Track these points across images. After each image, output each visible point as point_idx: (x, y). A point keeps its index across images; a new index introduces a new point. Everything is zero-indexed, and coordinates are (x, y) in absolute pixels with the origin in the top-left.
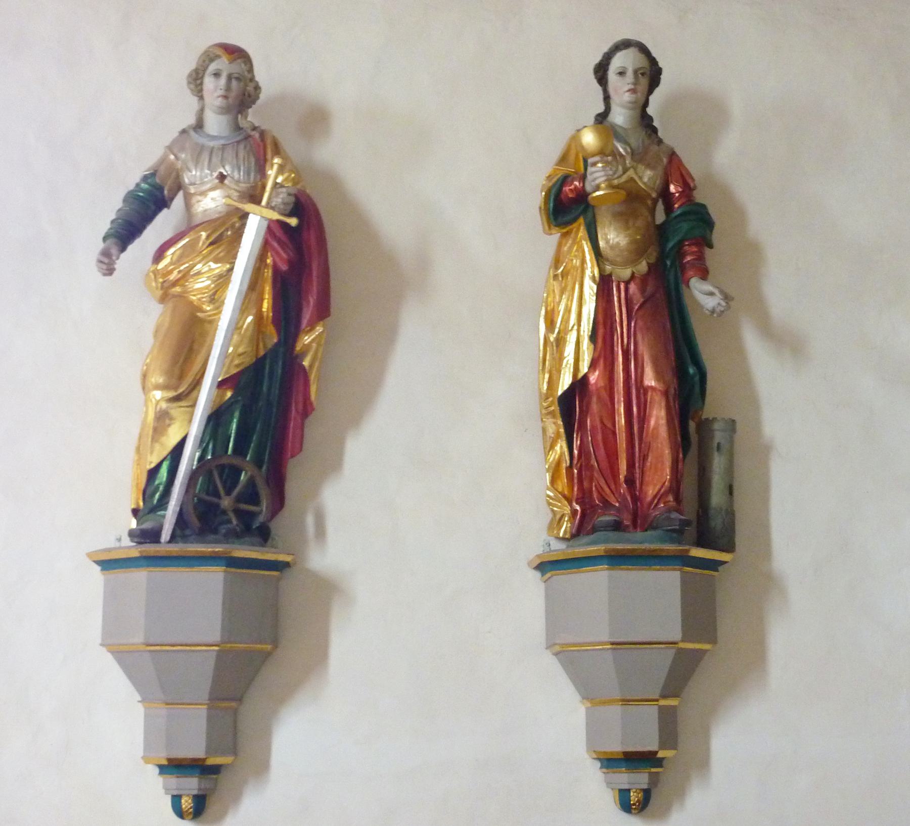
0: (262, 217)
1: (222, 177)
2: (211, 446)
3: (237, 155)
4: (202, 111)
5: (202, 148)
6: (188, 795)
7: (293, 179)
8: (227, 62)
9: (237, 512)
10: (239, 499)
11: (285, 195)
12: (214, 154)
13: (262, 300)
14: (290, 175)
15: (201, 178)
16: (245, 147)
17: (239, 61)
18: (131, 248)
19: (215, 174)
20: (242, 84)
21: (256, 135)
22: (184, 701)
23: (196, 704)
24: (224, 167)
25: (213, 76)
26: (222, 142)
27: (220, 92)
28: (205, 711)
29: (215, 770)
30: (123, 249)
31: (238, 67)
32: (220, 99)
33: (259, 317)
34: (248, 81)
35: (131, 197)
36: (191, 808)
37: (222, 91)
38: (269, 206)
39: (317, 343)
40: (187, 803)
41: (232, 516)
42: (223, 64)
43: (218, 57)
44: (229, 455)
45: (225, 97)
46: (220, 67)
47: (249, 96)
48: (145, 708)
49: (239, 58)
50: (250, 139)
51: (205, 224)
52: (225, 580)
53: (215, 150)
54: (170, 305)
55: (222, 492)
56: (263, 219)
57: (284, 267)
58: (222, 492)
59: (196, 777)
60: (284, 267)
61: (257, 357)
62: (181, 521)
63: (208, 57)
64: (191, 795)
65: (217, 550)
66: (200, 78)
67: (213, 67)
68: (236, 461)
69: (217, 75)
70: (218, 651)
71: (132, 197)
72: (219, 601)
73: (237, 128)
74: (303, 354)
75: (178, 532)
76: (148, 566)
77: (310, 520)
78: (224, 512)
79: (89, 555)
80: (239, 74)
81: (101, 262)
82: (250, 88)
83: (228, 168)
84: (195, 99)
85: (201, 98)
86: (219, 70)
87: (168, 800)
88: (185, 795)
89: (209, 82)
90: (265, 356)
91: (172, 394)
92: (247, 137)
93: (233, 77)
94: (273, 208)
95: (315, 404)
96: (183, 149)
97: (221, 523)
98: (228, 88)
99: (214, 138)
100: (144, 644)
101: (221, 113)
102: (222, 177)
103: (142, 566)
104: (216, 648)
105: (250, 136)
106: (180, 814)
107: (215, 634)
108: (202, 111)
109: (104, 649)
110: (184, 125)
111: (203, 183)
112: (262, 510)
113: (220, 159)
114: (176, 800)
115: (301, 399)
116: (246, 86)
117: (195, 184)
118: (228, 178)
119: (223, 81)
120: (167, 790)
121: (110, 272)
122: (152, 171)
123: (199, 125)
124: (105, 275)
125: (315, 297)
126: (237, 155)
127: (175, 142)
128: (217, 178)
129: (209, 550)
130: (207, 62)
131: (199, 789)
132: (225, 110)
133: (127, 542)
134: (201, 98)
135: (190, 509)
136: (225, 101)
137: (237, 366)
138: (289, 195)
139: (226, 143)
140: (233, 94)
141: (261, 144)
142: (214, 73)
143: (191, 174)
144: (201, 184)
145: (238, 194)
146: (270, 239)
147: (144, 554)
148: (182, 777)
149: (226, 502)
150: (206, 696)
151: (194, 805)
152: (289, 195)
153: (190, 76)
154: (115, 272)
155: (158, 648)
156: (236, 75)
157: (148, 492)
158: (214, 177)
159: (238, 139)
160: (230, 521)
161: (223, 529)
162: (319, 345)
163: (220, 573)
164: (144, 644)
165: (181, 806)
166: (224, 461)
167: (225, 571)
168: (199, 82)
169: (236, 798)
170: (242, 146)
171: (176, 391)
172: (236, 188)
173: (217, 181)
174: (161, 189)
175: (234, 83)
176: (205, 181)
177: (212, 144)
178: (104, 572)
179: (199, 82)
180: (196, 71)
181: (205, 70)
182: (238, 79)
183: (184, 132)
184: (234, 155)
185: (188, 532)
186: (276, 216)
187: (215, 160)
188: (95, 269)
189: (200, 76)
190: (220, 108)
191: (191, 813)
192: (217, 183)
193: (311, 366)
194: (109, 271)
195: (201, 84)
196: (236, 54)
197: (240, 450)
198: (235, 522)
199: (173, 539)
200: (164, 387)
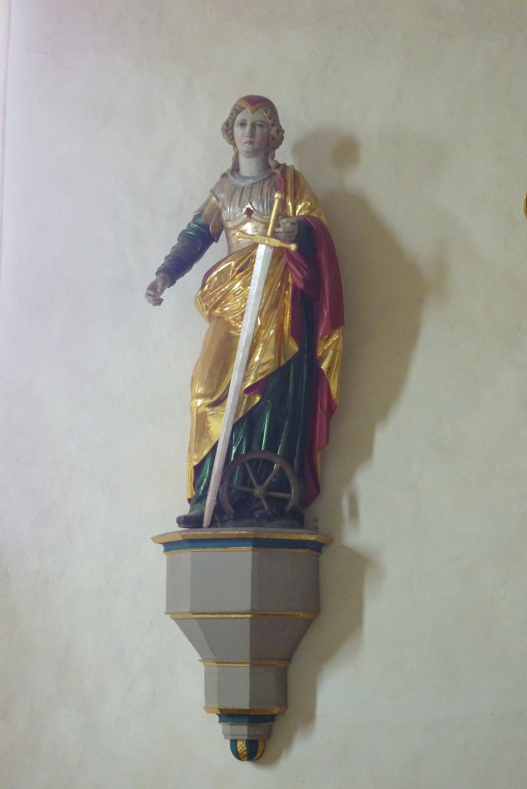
0: (268, 245)
1: (249, 212)
2: (244, 444)
3: (262, 191)
4: (237, 156)
5: (236, 187)
6: (242, 740)
7: (310, 206)
8: (250, 112)
9: (268, 498)
10: (270, 488)
11: (288, 225)
12: (244, 192)
13: (285, 315)
14: (307, 204)
15: (234, 214)
16: (270, 184)
17: (260, 110)
18: (180, 282)
19: (244, 210)
20: (265, 130)
21: (278, 172)
22: (232, 660)
23: (237, 663)
24: (251, 204)
25: (239, 126)
26: (251, 181)
27: (247, 139)
28: (249, 669)
29: (272, 718)
30: (172, 282)
31: (261, 115)
32: (247, 145)
33: (279, 331)
34: (270, 125)
35: (184, 236)
36: (245, 751)
37: (248, 138)
38: (274, 235)
39: (333, 350)
40: (241, 746)
41: (264, 502)
42: (247, 115)
43: (243, 108)
44: (262, 451)
45: (251, 143)
46: (243, 118)
47: (273, 138)
48: (206, 666)
49: (261, 107)
50: (275, 176)
51: (235, 254)
52: (254, 558)
53: (246, 188)
54: (214, 323)
55: (255, 484)
56: (268, 248)
57: (301, 286)
58: (255, 484)
59: (245, 725)
60: (301, 286)
61: (279, 366)
62: (218, 510)
63: (237, 110)
64: (245, 740)
65: (242, 532)
66: (230, 129)
67: (239, 118)
68: (268, 456)
69: (243, 124)
70: (251, 618)
71: (185, 237)
72: (249, 575)
73: (266, 166)
74: (322, 359)
75: (217, 518)
76: (191, 547)
77: (345, 503)
78: (258, 500)
79: (155, 539)
80: (261, 121)
81: (150, 295)
82: (273, 132)
83: (254, 204)
84: (232, 146)
85: (235, 145)
86: (245, 120)
87: (227, 743)
88: (239, 740)
89: (238, 132)
90: (288, 364)
91: (209, 401)
92: (272, 175)
93: (256, 124)
94: (276, 238)
95: (337, 402)
96: (222, 191)
97: (256, 509)
98: (252, 134)
99: (246, 178)
100: (190, 613)
101: (250, 157)
102: (249, 212)
103: (185, 548)
104: (249, 616)
105: (275, 174)
106: (238, 755)
107: (246, 604)
108: (237, 156)
109: (168, 616)
110: (225, 170)
111: (235, 218)
112: (291, 497)
113: (248, 197)
114: (234, 743)
115: (325, 399)
116: (269, 130)
117: (230, 220)
118: (255, 212)
119: (247, 129)
120: (226, 736)
121: (159, 302)
122: (198, 213)
123: (236, 169)
124: (154, 305)
125: (328, 310)
126: (262, 191)
127: (218, 184)
128: (245, 213)
129: (236, 532)
130: (234, 115)
131: (249, 735)
132: (253, 153)
133: (176, 528)
134: (235, 145)
135: (225, 498)
136: (250, 146)
137: (262, 374)
138: (292, 224)
139: (254, 182)
140: (257, 139)
141: (282, 180)
142: (240, 123)
143: (226, 212)
144: (234, 219)
145: (263, 225)
146: (289, 263)
147: (186, 538)
148: (235, 725)
149: (258, 491)
150: (248, 657)
151: (246, 749)
152: (292, 224)
153: (223, 128)
154: (163, 302)
155: (202, 616)
156: (259, 123)
157: (197, 484)
158: (243, 212)
159: (264, 177)
160: (262, 507)
161: (257, 514)
162: (335, 351)
163: (249, 552)
164: (190, 613)
165: (237, 749)
166: (255, 456)
167: (253, 550)
168: (230, 132)
169: (288, 743)
170: (267, 183)
171: (211, 399)
172: (260, 219)
173: (246, 216)
174: (207, 227)
175: (258, 130)
176: (237, 217)
177: (243, 184)
178: (166, 553)
179: (230, 132)
180: (227, 124)
181: (233, 122)
182: (261, 126)
183: (224, 175)
184: (260, 193)
185: (226, 518)
186: (277, 243)
187: (245, 197)
188: (146, 300)
189: (230, 126)
190: (248, 152)
191: (245, 755)
192: (246, 217)
193: (329, 368)
194: (158, 302)
195: (232, 133)
196: (258, 104)
197: (272, 446)
198: (266, 507)
199: (211, 526)
200: (203, 396)
